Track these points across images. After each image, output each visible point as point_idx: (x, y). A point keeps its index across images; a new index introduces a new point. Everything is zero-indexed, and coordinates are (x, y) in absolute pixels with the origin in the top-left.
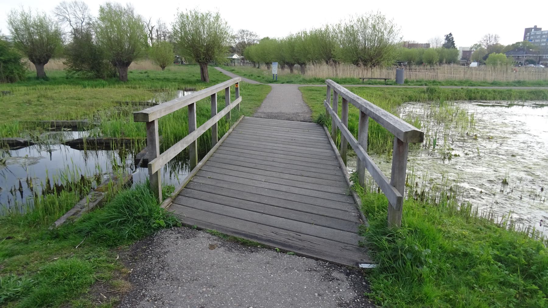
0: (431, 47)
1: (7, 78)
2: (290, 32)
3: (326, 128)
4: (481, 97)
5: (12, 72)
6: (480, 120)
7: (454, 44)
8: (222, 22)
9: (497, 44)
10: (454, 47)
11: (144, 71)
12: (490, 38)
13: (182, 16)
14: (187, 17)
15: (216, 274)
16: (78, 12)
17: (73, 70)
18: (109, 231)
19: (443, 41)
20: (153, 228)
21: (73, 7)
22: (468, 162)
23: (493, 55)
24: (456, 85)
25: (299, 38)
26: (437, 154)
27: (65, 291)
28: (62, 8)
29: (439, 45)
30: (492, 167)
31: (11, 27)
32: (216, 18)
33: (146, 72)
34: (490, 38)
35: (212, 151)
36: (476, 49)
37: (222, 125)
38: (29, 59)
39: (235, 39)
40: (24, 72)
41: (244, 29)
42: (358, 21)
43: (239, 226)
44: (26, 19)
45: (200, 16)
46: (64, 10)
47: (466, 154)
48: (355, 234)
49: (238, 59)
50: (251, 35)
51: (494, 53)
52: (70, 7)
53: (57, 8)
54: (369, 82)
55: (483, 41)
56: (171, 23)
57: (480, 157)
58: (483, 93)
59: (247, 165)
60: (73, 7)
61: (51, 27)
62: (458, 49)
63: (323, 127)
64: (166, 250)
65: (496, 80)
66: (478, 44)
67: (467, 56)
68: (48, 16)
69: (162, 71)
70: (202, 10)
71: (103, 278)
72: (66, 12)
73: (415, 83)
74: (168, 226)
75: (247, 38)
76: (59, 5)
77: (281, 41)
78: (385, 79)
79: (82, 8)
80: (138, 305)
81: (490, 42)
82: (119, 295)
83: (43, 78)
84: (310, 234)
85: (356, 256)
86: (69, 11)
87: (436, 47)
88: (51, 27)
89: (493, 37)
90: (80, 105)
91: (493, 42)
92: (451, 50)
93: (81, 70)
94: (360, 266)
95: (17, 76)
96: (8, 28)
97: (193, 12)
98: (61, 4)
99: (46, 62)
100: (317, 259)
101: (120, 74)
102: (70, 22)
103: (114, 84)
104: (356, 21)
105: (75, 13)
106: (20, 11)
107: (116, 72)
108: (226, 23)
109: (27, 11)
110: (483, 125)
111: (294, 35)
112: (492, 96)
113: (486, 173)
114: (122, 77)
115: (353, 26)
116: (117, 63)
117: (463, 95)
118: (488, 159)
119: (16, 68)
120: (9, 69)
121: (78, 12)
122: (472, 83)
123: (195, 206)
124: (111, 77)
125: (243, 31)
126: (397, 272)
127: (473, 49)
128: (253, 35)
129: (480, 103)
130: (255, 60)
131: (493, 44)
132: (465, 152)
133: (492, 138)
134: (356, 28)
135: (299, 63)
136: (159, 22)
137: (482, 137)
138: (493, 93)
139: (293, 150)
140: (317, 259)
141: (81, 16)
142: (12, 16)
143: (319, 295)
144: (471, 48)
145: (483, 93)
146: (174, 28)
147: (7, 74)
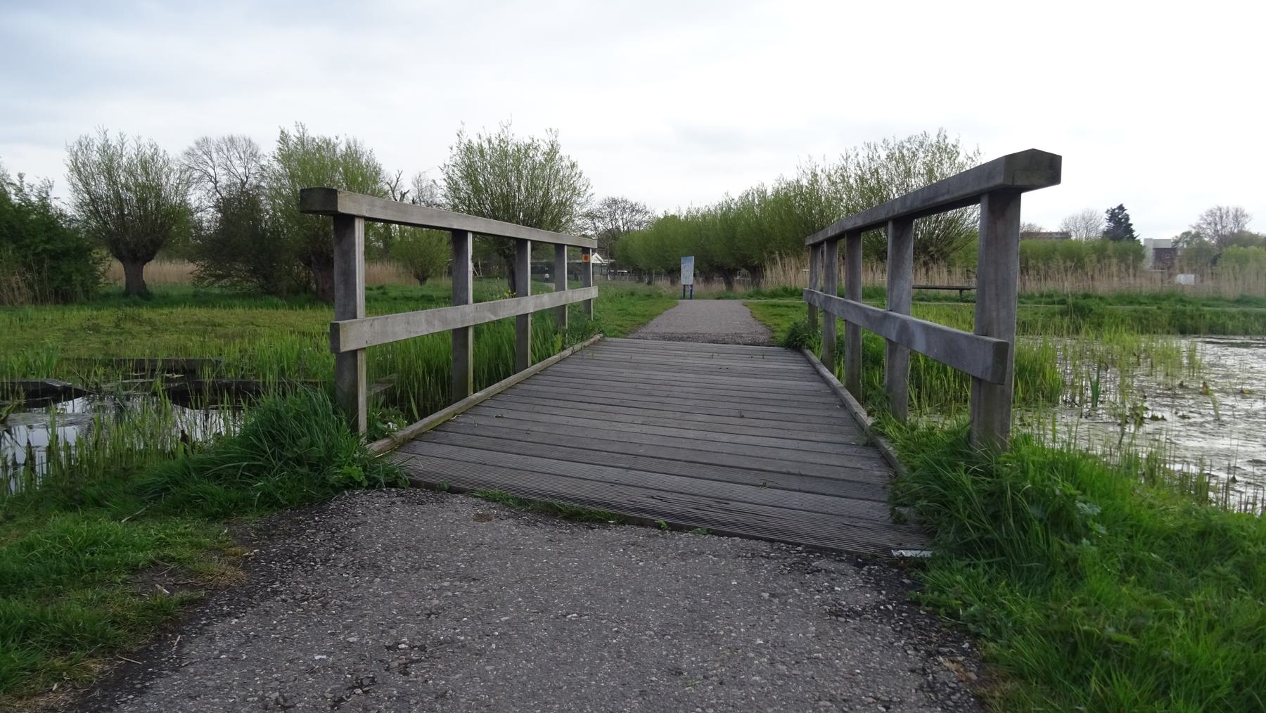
0: (1073, 238)
1: (56, 294)
2: (727, 194)
3: (808, 352)
4: (1211, 327)
5: (68, 280)
6: (1214, 365)
7: (1132, 231)
8: (563, 164)
9: (1241, 232)
10: (1133, 238)
11: (378, 285)
12: (1221, 217)
13: (469, 149)
14: (481, 151)
15: (483, 559)
16: (237, 162)
17: (211, 275)
18: (213, 487)
19: (1104, 225)
20: (333, 486)
21: (226, 151)
22: (1189, 430)
23: (1233, 249)
24: (1140, 304)
25: (746, 205)
26: (1105, 416)
27: (60, 572)
28: (200, 153)
29: (1093, 235)
30: (1258, 440)
31: (75, 180)
32: (548, 154)
33: (381, 287)
34: (1221, 217)
35: (513, 379)
36: (1188, 243)
37: (545, 340)
38: (111, 251)
39: (596, 221)
40: (96, 280)
41: (617, 195)
42: (890, 157)
43: (562, 487)
44: (111, 160)
45: (510, 149)
46: (205, 157)
47: (1183, 417)
48: (881, 504)
49: (601, 266)
50: (633, 211)
51: (1235, 245)
52: (219, 150)
53: (189, 154)
54: (920, 297)
55: (1204, 226)
56: (442, 166)
57: (1222, 424)
58: (1214, 318)
59: (599, 401)
60: (226, 151)
61: (167, 177)
62: (1142, 243)
63: (804, 355)
64: (358, 521)
65: (1247, 294)
66: (1193, 232)
67: (1165, 254)
68: (161, 154)
69: (419, 287)
70: (520, 135)
71: (172, 559)
72: (209, 161)
73: (1036, 300)
74: (373, 485)
75: (625, 216)
76: (194, 146)
77: (704, 216)
78: (961, 290)
79: (244, 152)
80: (253, 607)
81: (1223, 227)
82: (206, 589)
83: (140, 295)
84: (756, 501)
85: (886, 539)
86: (215, 159)
87: (1087, 239)
88: (167, 177)
89: (1231, 216)
90: (212, 335)
91: (1231, 227)
92: (1125, 244)
93: (228, 275)
94: (895, 553)
95: (79, 289)
96: (69, 179)
97: (496, 142)
98: (198, 143)
99: (149, 257)
100: (772, 541)
101: (317, 286)
102: (216, 185)
103: (302, 307)
104: (883, 156)
105: (229, 163)
106: (98, 142)
107: (308, 282)
108: (573, 166)
109: (114, 142)
110: (1223, 373)
111: (736, 199)
112: (1241, 325)
113: (1243, 449)
114: (323, 291)
115: (876, 171)
116: (313, 258)
117: (1165, 318)
118: (1243, 425)
119: (78, 270)
120: (62, 273)
121: (237, 162)
122: (1184, 298)
123: (452, 456)
124: (296, 292)
125: (615, 202)
126: (1003, 554)
127: (1181, 245)
128: (638, 211)
129: (1208, 340)
130: (641, 265)
131: (1232, 233)
132: (1181, 413)
133: (1251, 392)
134: (885, 177)
135: (746, 267)
136: (418, 182)
137: (1222, 391)
138: (1242, 319)
139: (720, 382)
140: (772, 541)
141: (241, 170)
142: (79, 154)
143: (772, 595)
144: (1176, 242)
145: (1214, 318)
146: (450, 177)
147: (56, 284)
